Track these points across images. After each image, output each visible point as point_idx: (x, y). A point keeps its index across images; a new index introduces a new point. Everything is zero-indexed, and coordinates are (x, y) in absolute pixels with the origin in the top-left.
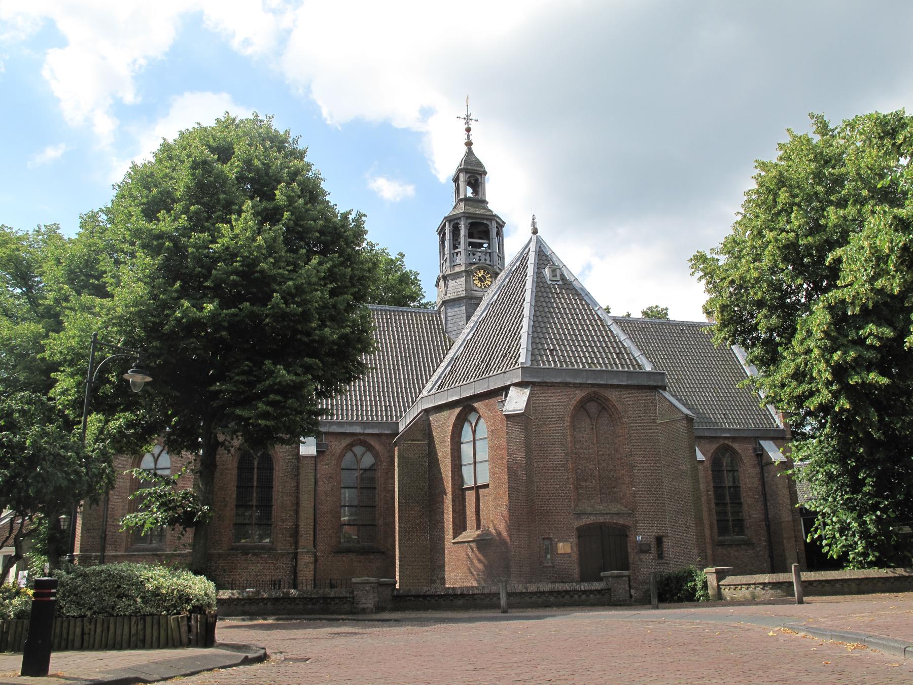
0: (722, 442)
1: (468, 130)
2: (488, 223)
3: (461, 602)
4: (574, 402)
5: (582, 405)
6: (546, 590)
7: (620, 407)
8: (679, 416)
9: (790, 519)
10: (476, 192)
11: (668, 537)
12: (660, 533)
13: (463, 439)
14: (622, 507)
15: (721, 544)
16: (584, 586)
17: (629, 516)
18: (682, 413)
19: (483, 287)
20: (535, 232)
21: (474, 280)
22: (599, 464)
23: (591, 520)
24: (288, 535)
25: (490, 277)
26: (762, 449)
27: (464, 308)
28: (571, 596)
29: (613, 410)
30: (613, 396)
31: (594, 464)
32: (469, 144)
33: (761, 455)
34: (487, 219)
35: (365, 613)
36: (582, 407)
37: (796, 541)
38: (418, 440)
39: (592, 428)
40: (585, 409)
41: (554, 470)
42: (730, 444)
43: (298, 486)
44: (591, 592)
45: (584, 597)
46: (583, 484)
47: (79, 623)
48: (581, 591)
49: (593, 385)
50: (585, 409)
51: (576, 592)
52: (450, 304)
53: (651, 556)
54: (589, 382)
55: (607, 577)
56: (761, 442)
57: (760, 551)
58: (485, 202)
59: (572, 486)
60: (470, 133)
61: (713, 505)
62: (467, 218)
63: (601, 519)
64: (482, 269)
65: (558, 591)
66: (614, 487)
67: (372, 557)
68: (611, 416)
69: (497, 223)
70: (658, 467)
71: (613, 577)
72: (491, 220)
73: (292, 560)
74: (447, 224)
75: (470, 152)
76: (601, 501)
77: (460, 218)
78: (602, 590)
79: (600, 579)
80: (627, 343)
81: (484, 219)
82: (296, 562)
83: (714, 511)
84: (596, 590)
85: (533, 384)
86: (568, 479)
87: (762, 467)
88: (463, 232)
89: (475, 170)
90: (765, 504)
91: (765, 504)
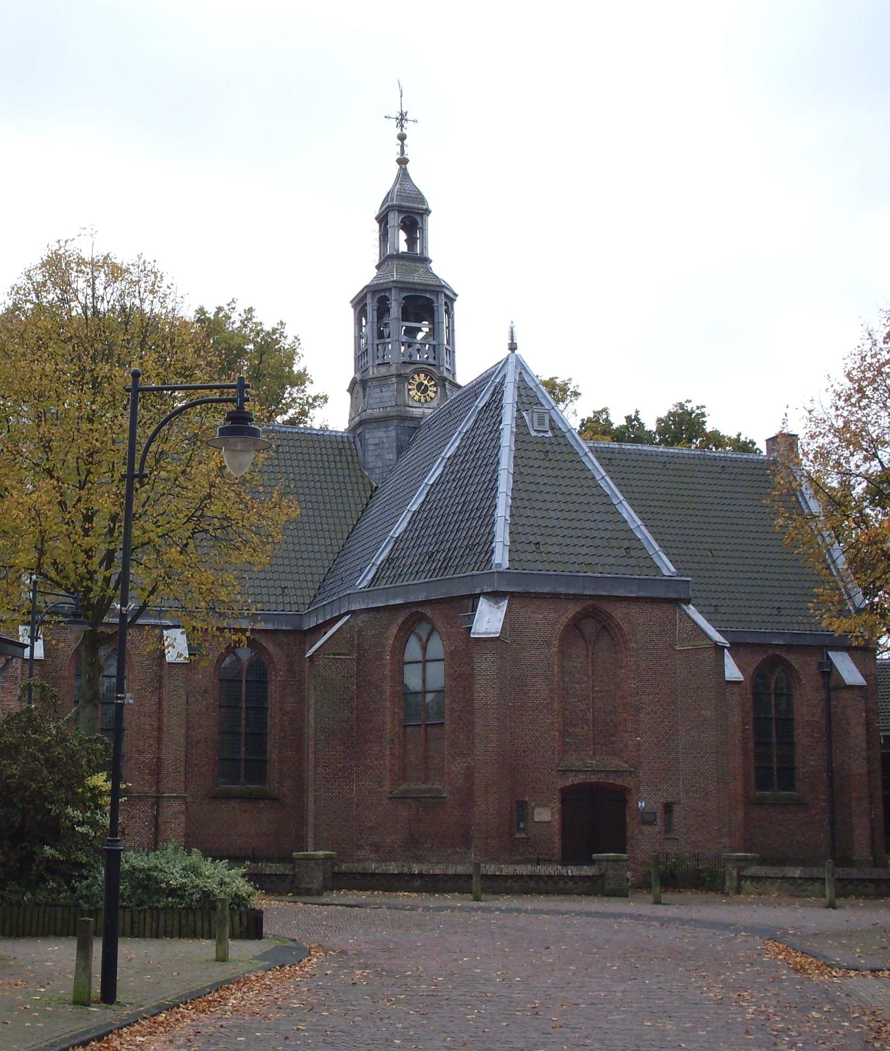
0: (770, 652)
1: (402, 138)
2: (433, 297)
3: (418, 883)
4: (564, 620)
5: (575, 625)
6: (524, 873)
7: (625, 626)
8: (705, 644)
9: (865, 770)
10: (411, 242)
11: (680, 804)
12: (670, 799)
13: (408, 657)
14: (621, 763)
15: (760, 803)
16: (572, 871)
17: (631, 774)
18: (711, 639)
19: (423, 400)
20: (513, 347)
21: (410, 390)
22: (593, 703)
23: (580, 778)
24: (147, 771)
25: (435, 385)
26: (831, 664)
27: (394, 433)
28: (556, 883)
29: (616, 630)
30: (618, 612)
31: (587, 704)
32: (403, 161)
33: (828, 674)
34: (431, 292)
35: (309, 895)
36: (575, 625)
37: (871, 803)
38: (343, 654)
39: (587, 655)
40: (578, 628)
41: (533, 711)
42: (783, 655)
43: (160, 703)
44: (581, 878)
45: (570, 884)
46: (572, 730)
47: (128, 914)
48: (568, 876)
49: (591, 597)
50: (578, 628)
51: (561, 877)
52: (370, 426)
53: (657, 829)
54: (587, 593)
55: (601, 860)
56: (830, 653)
57: (816, 814)
58: (426, 260)
59: (556, 733)
60: (405, 142)
61: (751, 745)
62: (402, 289)
63: (593, 778)
64: (423, 372)
65: (539, 876)
66: (612, 736)
67: (262, 805)
68: (613, 638)
69: (446, 296)
70: (673, 710)
71: (608, 860)
72: (437, 293)
73: (152, 806)
74: (369, 296)
75: (403, 176)
76: (594, 754)
77: (390, 289)
78: (593, 876)
79: (591, 862)
80: (643, 533)
81: (426, 291)
82: (158, 810)
83: (752, 754)
84: (586, 876)
85: (512, 595)
86: (553, 723)
87: (829, 691)
88: (395, 310)
89: (413, 208)
90: (829, 746)
91: (829, 746)
